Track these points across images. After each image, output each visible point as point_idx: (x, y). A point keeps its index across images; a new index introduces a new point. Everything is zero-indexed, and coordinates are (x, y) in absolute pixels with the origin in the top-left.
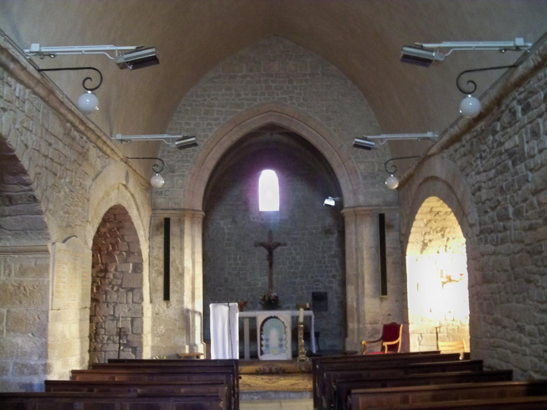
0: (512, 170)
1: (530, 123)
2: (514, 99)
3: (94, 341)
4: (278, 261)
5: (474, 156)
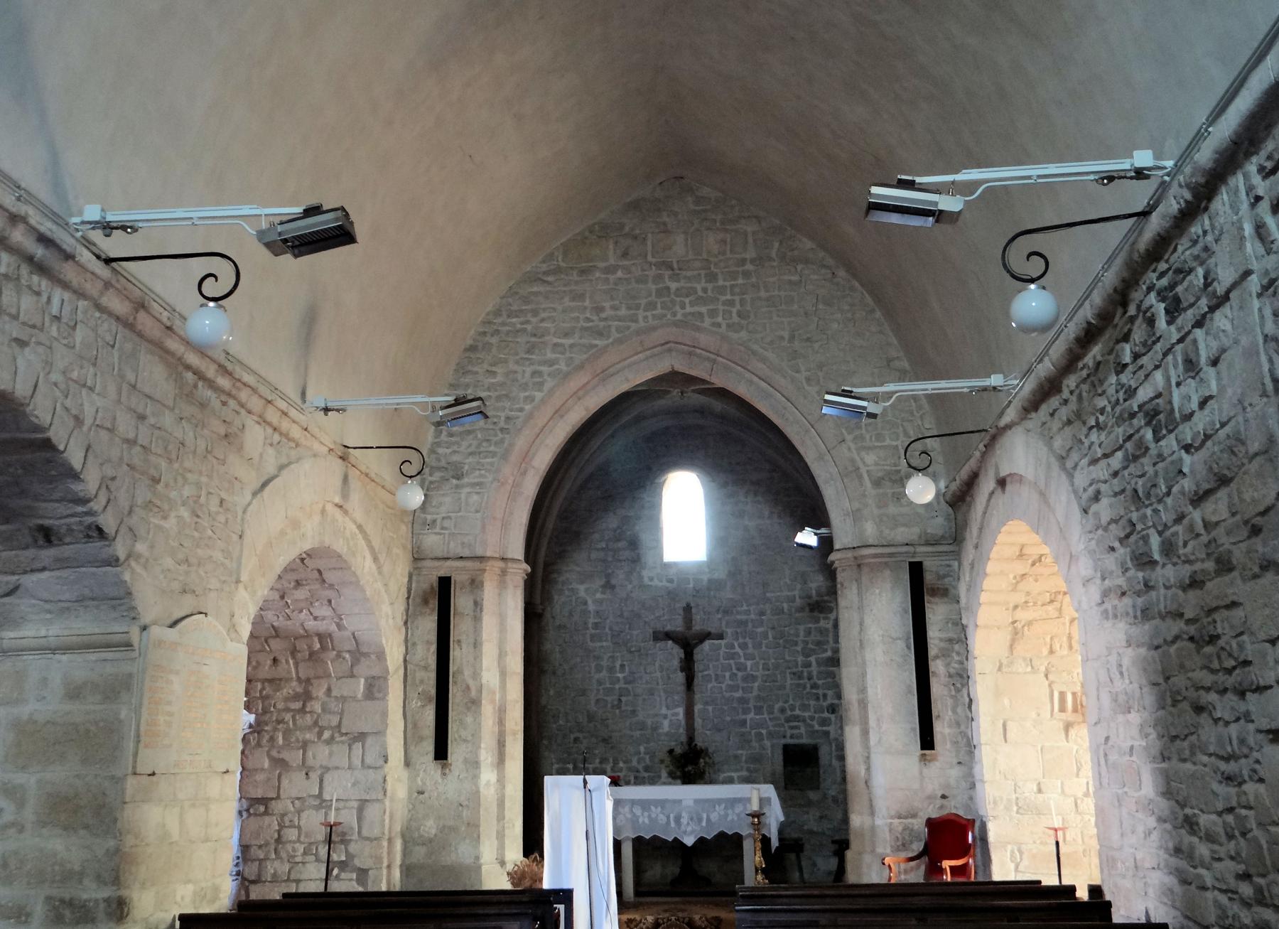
0: (1153, 451)
1: (1181, 340)
2: (1150, 289)
3: (273, 856)
4: (706, 673)
5: (1084, 423)
